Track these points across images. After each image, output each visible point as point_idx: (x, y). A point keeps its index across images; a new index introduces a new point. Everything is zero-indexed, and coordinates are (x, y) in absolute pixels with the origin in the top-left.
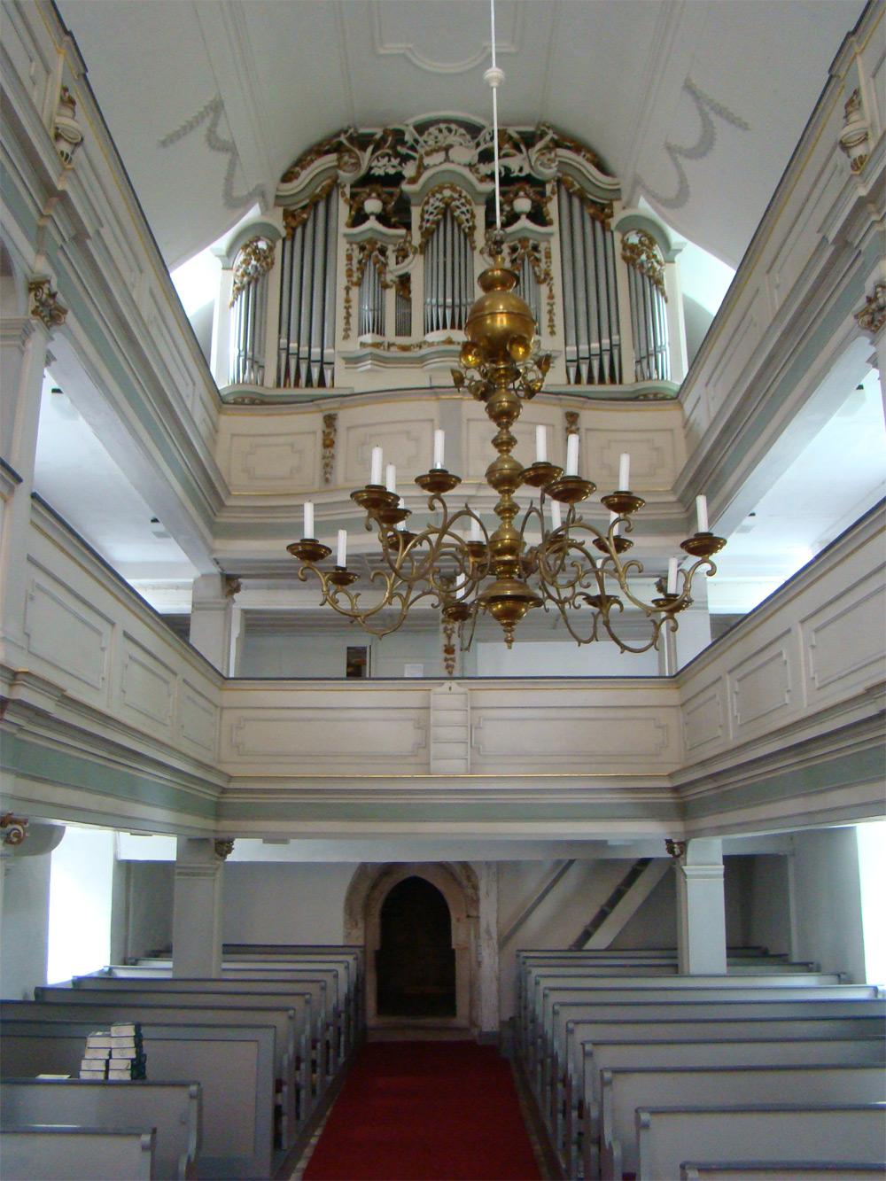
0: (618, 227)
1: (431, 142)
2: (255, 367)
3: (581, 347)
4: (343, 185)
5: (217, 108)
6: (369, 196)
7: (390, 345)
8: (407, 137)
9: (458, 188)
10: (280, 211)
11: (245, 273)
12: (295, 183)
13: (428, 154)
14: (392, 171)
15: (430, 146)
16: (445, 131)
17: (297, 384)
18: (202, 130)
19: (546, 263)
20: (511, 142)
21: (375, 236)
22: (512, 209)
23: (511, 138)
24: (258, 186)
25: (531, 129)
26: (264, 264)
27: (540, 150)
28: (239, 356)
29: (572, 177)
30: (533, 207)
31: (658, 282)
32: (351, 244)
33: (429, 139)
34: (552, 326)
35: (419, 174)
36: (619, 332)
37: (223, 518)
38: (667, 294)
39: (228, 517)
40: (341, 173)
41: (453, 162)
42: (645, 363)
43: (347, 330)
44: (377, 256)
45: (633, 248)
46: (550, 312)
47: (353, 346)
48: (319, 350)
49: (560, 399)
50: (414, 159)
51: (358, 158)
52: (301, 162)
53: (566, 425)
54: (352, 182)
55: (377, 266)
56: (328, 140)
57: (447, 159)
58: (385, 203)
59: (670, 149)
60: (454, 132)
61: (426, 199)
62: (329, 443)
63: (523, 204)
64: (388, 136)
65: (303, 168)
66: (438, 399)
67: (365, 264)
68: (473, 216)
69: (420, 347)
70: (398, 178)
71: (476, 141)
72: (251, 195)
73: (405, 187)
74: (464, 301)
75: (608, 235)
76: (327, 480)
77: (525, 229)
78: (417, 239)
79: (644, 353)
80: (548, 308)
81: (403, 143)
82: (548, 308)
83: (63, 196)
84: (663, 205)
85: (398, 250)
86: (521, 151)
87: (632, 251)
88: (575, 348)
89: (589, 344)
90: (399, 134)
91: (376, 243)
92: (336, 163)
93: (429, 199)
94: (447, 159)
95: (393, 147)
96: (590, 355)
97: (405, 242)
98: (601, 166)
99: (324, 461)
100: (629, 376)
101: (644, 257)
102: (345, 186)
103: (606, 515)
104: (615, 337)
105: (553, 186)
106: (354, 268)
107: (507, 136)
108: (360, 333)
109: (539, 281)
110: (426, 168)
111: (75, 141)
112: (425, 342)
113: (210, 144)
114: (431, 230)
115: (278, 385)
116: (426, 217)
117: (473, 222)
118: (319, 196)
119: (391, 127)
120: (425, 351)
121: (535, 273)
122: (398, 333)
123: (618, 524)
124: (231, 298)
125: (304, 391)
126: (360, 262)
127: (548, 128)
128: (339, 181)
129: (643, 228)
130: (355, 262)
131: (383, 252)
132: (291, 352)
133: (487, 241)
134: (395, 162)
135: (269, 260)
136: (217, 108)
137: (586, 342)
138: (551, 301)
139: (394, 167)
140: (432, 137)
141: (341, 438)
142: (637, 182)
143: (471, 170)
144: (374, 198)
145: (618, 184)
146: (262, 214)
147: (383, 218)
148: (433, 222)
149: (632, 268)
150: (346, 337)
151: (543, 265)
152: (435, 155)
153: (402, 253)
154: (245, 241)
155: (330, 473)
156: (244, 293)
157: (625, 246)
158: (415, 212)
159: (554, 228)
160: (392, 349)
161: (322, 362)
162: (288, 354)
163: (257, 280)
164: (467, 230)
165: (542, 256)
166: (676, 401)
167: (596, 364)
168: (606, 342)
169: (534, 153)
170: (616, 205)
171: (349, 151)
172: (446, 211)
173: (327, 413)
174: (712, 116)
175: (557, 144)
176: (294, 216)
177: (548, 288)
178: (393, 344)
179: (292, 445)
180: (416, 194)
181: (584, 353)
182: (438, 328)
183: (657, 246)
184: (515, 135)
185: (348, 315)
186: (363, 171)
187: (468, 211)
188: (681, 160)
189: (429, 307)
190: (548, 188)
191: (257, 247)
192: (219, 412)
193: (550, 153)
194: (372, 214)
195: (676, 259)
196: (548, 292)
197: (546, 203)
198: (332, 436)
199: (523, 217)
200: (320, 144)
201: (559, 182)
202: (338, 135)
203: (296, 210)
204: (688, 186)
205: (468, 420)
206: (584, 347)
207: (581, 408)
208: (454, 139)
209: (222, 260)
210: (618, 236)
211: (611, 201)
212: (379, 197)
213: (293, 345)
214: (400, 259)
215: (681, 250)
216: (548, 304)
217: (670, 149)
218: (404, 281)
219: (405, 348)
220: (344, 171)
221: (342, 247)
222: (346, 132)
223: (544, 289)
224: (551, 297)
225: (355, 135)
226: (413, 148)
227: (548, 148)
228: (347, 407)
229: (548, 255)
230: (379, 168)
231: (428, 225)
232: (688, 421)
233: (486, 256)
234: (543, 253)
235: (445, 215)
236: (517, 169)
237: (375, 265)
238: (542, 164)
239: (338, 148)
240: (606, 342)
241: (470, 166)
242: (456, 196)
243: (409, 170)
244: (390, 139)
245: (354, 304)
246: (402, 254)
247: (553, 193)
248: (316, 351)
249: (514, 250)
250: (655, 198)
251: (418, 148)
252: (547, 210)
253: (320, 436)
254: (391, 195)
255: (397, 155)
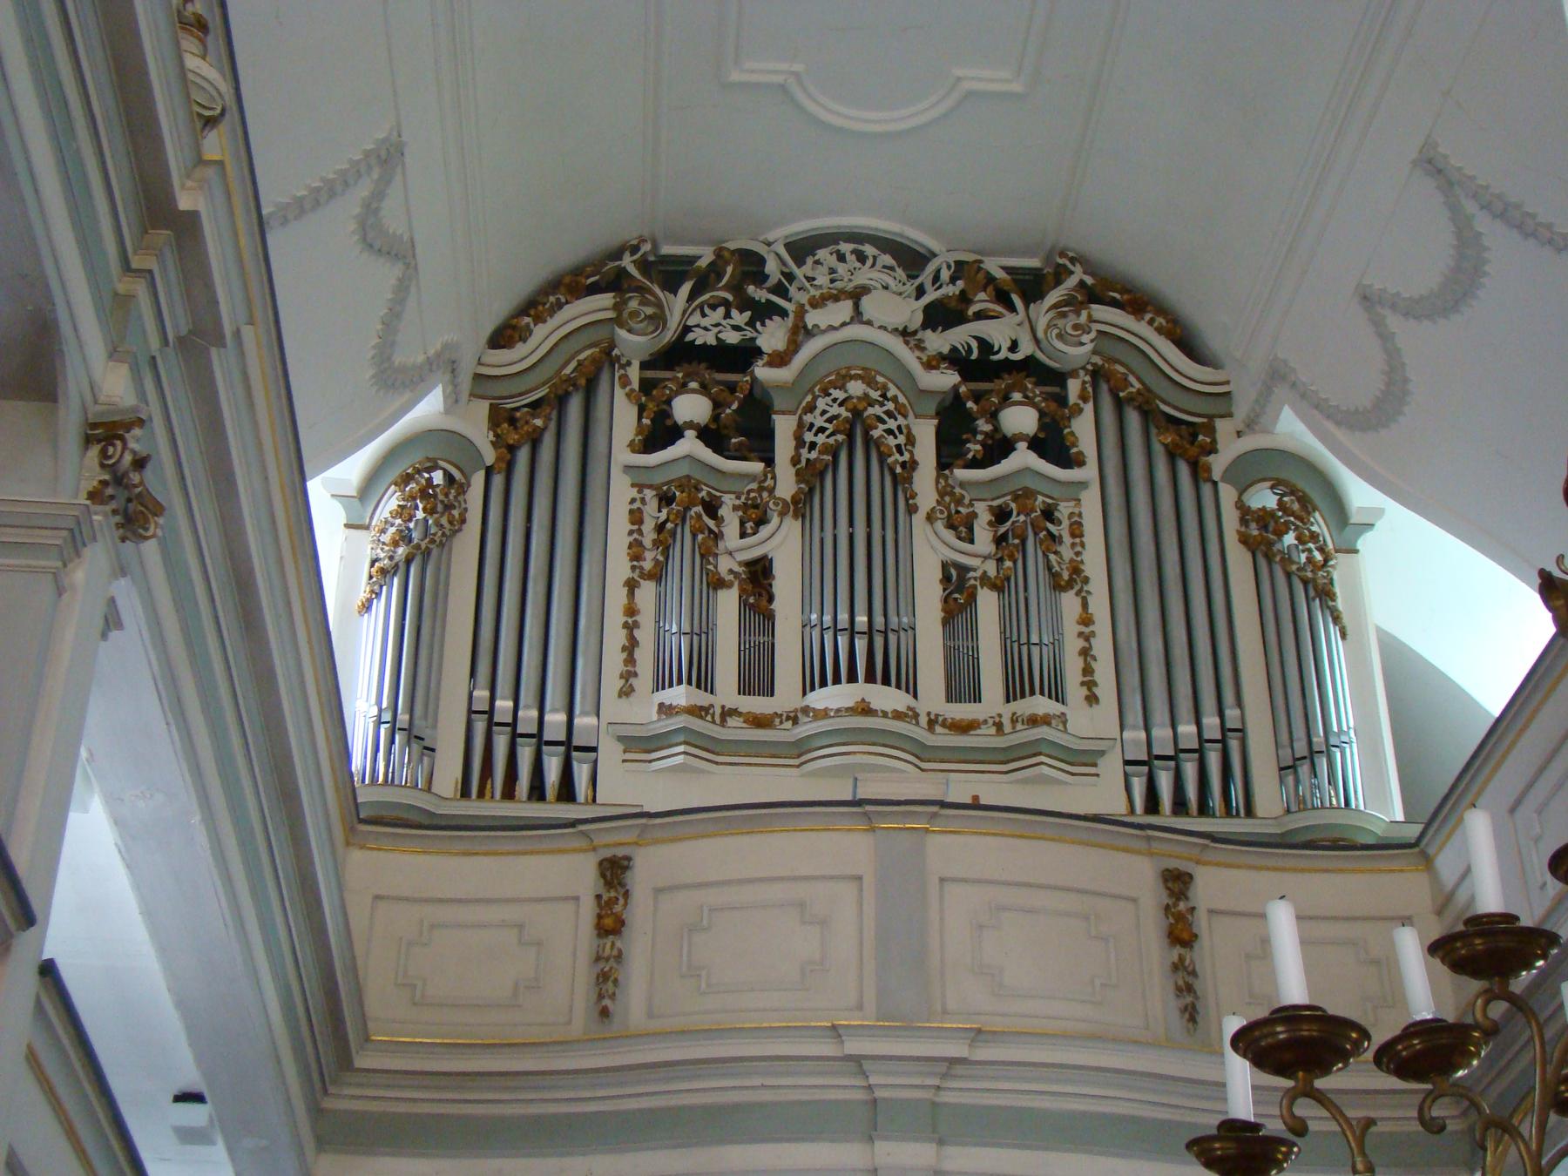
0: (1228, 476)
1: (823, 280)
2: (416, 747)
3: (1155, 732)
4: (624, 361)
5: (389, 157)
6: (683, 388)
7: (727, 713)
8: (772, 267)
9: (880, 379)
10: (483, 407)
11: (404, 537)
12: (521, 349)
13: (816, 304)
14: (732, 338)
15: (820, 287)
16: (851, 258)
17: (509, 793)
18: (349, 206)
19: (1073, 545)
20: (990, 289)
21: (697, 475)
22: (997, 429)
23: (990, 279)
24: (447, 346)
25: (1033, 263)
26: (444, 521)
27: (1055, 306)
28: (379, 722)
29: (1122, 364)
30: (1042, 426)
31: (1325, 594)
32: (640, 487)
33: (820, 271)
34: (1090, 685)
35: (794, 346)
36: (1239, 703)
37: (347, 1100)
38: (1346, 620)
39: (353, 1097)
40: (622, 333)
41: (869, 323)
42: (1304, 769)
43: (629, 675)
44: (699, 516)
45: (1264, 517)
46: (1085, 653)
47: (642, 711)
48: (561, 717)
49: (1149, 838)
50: (783, 313)
51: (659, 305)
52: (535, 307)
53: (1166, 900)
54: (647, 358)
55: (700, 537)
56: (596, 264)
57: (858, 316)
58: (717, 405)
59: (1367, 299)
60: (869, 262)
61: (809, 398)
62: (610, 924)
63: (1020, 419)
64: (727, 263)
65: (539, 319)
66: (873, 830)
67: (673, 534)
68: (911, 440)
69: (795, 721)
70: (746, 355)
71: (917, 282)
72: (431, 364)
73: (762, 372)
74: (894, 620)
75: (1207, 489)
76: (605, 1013)
77: (1027, 471)
78: (786, 484)
79: (1301, 748)
80: (1081, 643)
81: (760, 278)
82: (1081, 643)
83: (186, 228)
84: (1338, 423)
85: (745, 507)
86: (1012, 308)
87: (1264, 527)
88: (1143, 735)
89: (1174, 727)
90: (751, 265)
91: (699, 490)
92: (611, 314)
93: (815, 398)
94: (858, 316)
95: (737, 288)
96: (1179, 751)
97: (761, 489)
98: (1188, 344)
99: (597, 969)
100: (1269, 795)
101: (1290, 539)
102: (629, 363)
103: (1262, 1116)
104: (1232, 713)
105: (1084, 383)
106: (647, 542)
107: (981, 276)
108: (660, 684)
109: (1058, 585)
110: (810, 334)
111: (207, 113)
112: (806, 710)
113: (364, 238)
114: (819, 466)
115: (465, 793)
116: (809, 437)
117: (911, 453)
118: (569, 380)
119: (732, 246)
120: (806, 728)
121: (1049, 568)
122: (745, 688)
123: (1340, 1129)
124: (363, 592)
125: (523, 809)
126: (660, 528)
127: (1072, 261)
128: (616, 352)
129: (1284, 475)
130: (649, 527)
131: (712, 508)
132: (497, 719)
133: (942, 494)
134: (740, 318)
135: (456, 513)
136: (389, 157)
137: (1192, 717)
138: (1087, 630)
139: (736, 328)
140: (824, 270)
141: (640, 910)
142: (1277, 376)
143: (907, 343)
144: (693, 391)
145: (1228, 383)
146: (448, 411)
147: (711, 436)
148: (826, 449)
149: (1262, 562)
150: (626, 692)
151: (1067, 552)
152: (831, 306)
153: (753, 513)
154: (404, 466)
155: (613, 996)
156: (396, 580)
157: (1245, 514)
158: (784, 427)
159: (1089, 472)
160: (732, 722)
161: (569, 746)
162: (491, 724)
163: (427, 554)
164: (899, 470)
165: (1063, 530)
166: (1416, 850)
167: (1190, 770)
168: (1211, 722)
169: (1042, 312)
170: (1222, 426)
171: (641, 289)
172: (855, 425)
173: (608, 853)
174: (1483, 223)
175: (1092, 295)
176: (513, 421)
177: (1078, 601)
178: (734, 712)
179: (520, 927)
180: (781, 387)
181: (1163, 746)
182: (837, 680)
183: (1317, 515)
184: (1000, 274)
185: (631, 646)
186: (669, 335)
187: (899, 428)
188: (1393, 322)
189: (816, 633)
190: (1074, 387)
191: (430, 480)
192: (348, 844)
193: (1078, 314)
194: (690, 425)
195: (1360, 545)
196: (1078, 608)
197: (1069, 419)
198: (618, 908)
199: (1022, 446)
200: (578, 271)
201: (1097, 374)
202: (617, 254)
203: (517, 409)
204: (1406, 380)
205: (942, 880)
206: (1162, 733)
207: (1198, 862)
208: (875, 274)
209: (346, 508)
210: (1228, 494)
211: (1211, 417)
212: (704, 389)
213: (504, 704)
214: (749, 525)
215: (1372, 525)
216: (1080, 634)
217: (1367, 299)
218: (759, 574)
219: (759, 722)
220: (629, 331)
221: (622, 493)
222: (635, 249)
223: (1069, 603)
224: (1086, 620)
225: (652, 258)
226: (780, 290)
227: (1071, 304)
228: (656, 842)
229: (1077, 530)
230: (706, 329)
231: (814, 455)
232: (1449, 898)
233: (939, 525)
234: (1066, 523)
235: (851, 437)
236: (1006, 344)
237: (694, 536)
238: (1060, 337)
239: (617, 283)
240: (1211, 722)
241: (905, 333)
242: (875, 395)
243: (772, 337)
244: (729, 269)
245: (647, 618)
246: (755, 517)
247: (1084, 398)
248: (555, 718)
249: (1001, 515)
250: (1317, 409)
251: (792, 290)
252: (1072, 433)
253: (588, 909)
254: (732, 388)
255: (746, 303)
